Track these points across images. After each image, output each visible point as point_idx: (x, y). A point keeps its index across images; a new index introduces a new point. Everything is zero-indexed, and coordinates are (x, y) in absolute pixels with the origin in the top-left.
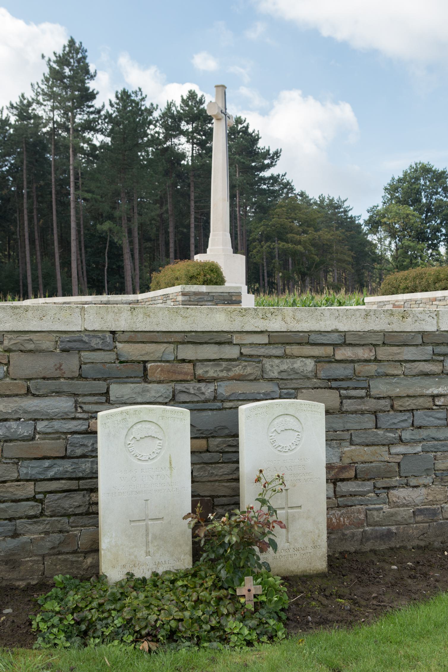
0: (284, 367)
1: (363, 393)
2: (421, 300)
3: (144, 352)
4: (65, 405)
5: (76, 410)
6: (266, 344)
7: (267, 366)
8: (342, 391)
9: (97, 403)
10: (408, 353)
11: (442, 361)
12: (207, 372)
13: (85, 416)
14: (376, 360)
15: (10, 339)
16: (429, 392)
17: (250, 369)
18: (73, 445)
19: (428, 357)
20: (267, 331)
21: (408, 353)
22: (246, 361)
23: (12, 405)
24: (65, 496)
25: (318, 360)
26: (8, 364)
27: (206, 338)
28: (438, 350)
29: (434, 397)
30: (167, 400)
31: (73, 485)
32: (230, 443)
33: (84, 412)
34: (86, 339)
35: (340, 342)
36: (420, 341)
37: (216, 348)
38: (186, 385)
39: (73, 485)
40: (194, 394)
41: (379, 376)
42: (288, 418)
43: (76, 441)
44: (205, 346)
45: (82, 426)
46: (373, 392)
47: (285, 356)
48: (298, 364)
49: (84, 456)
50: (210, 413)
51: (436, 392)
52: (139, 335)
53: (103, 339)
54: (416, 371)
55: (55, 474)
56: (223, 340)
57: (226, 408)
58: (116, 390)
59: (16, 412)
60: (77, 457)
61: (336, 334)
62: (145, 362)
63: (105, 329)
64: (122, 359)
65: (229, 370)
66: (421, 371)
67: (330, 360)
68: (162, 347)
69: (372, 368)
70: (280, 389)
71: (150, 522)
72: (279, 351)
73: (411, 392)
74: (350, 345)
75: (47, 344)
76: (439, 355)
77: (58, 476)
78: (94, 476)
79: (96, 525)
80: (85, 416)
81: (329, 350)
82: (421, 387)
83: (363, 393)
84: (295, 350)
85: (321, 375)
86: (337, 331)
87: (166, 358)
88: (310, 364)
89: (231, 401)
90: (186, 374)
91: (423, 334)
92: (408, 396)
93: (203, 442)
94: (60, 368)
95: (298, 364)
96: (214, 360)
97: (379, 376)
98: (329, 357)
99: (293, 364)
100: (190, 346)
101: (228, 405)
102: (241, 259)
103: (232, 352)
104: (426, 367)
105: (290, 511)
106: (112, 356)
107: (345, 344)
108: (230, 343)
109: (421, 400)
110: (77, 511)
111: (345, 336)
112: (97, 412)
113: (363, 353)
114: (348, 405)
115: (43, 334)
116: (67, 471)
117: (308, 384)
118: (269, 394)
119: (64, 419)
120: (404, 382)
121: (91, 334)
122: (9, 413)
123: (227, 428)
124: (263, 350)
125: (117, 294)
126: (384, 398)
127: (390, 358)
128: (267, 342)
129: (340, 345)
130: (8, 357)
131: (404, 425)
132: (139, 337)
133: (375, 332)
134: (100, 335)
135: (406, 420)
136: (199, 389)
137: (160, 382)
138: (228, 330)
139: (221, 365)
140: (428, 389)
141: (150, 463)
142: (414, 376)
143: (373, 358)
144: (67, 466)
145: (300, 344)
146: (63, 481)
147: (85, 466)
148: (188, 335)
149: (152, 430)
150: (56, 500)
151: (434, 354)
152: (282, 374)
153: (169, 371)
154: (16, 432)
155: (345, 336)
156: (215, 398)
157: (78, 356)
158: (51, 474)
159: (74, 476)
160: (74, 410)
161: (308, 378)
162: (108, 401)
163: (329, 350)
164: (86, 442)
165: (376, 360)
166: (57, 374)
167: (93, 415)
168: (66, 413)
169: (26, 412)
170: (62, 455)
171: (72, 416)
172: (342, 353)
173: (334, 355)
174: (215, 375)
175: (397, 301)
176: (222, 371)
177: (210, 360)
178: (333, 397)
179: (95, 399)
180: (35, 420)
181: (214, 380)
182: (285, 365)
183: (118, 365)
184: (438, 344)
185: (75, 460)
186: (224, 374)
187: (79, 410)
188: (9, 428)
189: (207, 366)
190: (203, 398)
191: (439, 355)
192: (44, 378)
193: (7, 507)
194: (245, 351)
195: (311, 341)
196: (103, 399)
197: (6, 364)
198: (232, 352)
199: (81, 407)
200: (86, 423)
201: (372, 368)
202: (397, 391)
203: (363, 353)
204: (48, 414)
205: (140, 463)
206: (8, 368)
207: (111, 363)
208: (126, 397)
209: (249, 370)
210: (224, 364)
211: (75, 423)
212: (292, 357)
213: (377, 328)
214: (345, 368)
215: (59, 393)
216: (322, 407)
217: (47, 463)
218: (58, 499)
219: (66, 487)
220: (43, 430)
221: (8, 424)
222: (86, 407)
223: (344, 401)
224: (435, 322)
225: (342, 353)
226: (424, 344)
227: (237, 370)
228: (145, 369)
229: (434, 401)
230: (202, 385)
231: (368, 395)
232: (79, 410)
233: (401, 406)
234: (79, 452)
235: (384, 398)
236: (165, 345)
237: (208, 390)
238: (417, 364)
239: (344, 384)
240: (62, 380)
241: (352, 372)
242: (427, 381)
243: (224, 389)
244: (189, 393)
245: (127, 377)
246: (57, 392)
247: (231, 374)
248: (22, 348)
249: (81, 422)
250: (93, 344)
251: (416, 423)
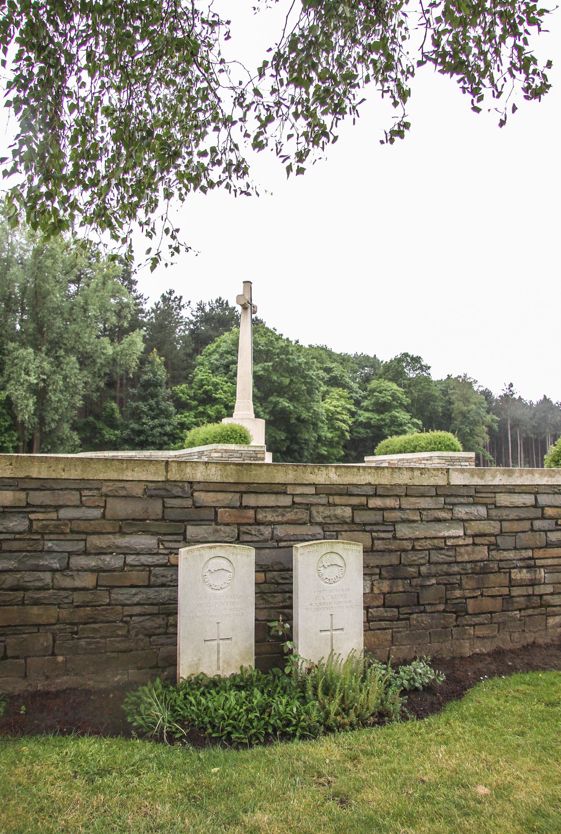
0: (327, 513)
1: (390, 535)
2: (412, 459)
3: (214, 500)
4: (150, 542)
5: (159, 547)
6: (313, 495)
7: (314, 513)
8: (373, 534)
9: (176, 541)
10: (424, 503)
11: (452, 510)
12: (266, 517)
13: (166, 552)
14: (400, 509)
15: (108, 486)
16: (441, 534)
17: (303, 515)
18: (156, 576)
19: (441, 506)
20: (314, 484)
21: (424, 503)
22: (297, 508)
23: (106, 541)
24: (148, 619)
25: (354, 508)
26: (105, 507)
27: (266, 488)
28: (448, 500)
29: (445, 538)
30: (233, 540)
31: (155, 609)
32: (283, 576)
33: (165, 548)
34: (169, 487)
35: (371, 493)
36: (434, 493)
37: (273, 497)
38: (249, 527)
39: (155, 609)
40: (255, 535)
41: (404, 521)
42: (334, 556)
43: (158, 572)
44: (265, 495)
45: (162, 560)
46: (399, 534)
47: (329, 504)
48: (339, 511)
49: (163, 585)
50: (267, 551)
51: (446, 534)
52: (212, 485)
53: (183, 488)
54: (431, 518)
55: (140, 600)
56: (279, 490)
57: (281, 547)
58: (191, 531)
59: (109, 547)
60: (158, 586)
61: (369, 487)
62: (215, 507)
63: (184, 480)
64: (198, 505)
65: (283, 515)
66: (436, 518)
67: (365, 507)
68: (230, 496)
69: (397, 515)
70: (324, 531)
71: (221, 642)
72: (324, 500)
73: (428, 535)
74: (380, 496)
75: (138, 491)
76: (450, 504)
77: (142, 602)
78: (174, 601)
79: (175, 644)
80: (166, 552)
81: (363, 500)
82: (435, 530)
83: (390, 535)
84: (337, 500)
85: (357, 520)
86: (369, 484)
87: (232, 504)
88: (348, 512)
89: (285, 541)
90: (249, 518)
91: (437, 487)
92: (426, 538)
93: (262, 575)
94: (146, 511)
95: (339, 511)
96: (272, 507)
97: (404, 521)
98: (364, 506)
99: (334, 511)
100: (253, 495)
101: (282, 544)
102: (261, 423)
103: (286, 501)
104: (439, 514)
105: (334, 632)
106: (189, 503)
107: (375, 495)
108: (285, 493)
109: (436, 541)
110: (158, 631)
111: (376, 488)
112: (178, 549)
113: (390, 502)
114: (379, 545)
115: (134, 483)
116: (149, 598)
117: (346, 527)
118: (315, 535)
119: (149, 554)
120: (422, 526)
121: (173, 483)
122: (104, 548)
123: (281, 564)
124: (311, 499)
125: (142, 449)
126: (406, 539)
127: (412, 507)
128: (314, 492)
129: (372, 496)
130: (105, 501)
131: (422, 561)
132: (212, 487)
133: (400, 485)
134: (180, 484)
135: (424, 557)
136: (259, 530)
137: (228, 524)
138: (283, 482)
139: (277, 511)
140: (440, 532)
141: (222, 591)
142: (430, 521)
143: (397, 507)
144: (151, 593)
145: (340, 495)
146: (146, 607)
147: (165, 593)
148: (251, 486)
149: (340, 562)
150: (140, 622)
151: (445, 503)
152: (327, 519)
153: (235, 516)
154: (109, 564)
155: (376, 488)
156: (272, 539)
157: (161, 501)
158: (136, 599)
159: (155, 601)
160: (157, 546)
161: (346, 523)
162: (185, 539)
163: (363, 500)
164: (165, 573)
165: (400, 509)
166: (144, 516)
167: (175, 551)
168: (150, 549)
169: (118, 547)
170: (146, 584)
171: (155, 551)
172: (375, 502)
173: (367, 504)
174: (272, 519)
175: (392, 460)
176: (278, 516)
177: (268, 507)
178: (367, 537)
179: (175, 537)
180: (125, 554)
181: (271, 523)
182: (328, 512)
183: (194, 510)
184: (448, 496)
185: (157, 589)
186: (280, 519)
187: (161, 547)
188: (104, 560)
189: (265, 512)
190: (262, 538)
191: (450, 504)
192: (133, 520)
193: (100, 627)
194: (297, 500)
195: (349, 493)
196: (181, 538)
197: (102, 507)
198: (286, 501)
199: (162, 544)
200: (167, 557)
201: (397, 515)
202: (417, 534)
203: (390, 502)
204: (136, 549)
205: (213, 591)
206: (104, 511)
207: (188, 508)
208: (200, 537)
209: (299, 516)
210: (280, 510)
211: (156, 557)
212: (335, 505)
213: (400, 482)
214: (376, 515)
215: (145, 532)
216: (361, 548)
217: (134, 591)
218: (143, 621)
219: (148, 611)
220: (132, 563)
221: (103, 557)
222: (167, 545)
223: (375, 542)
224: (446, 477)
225: (375, 502)
226: (437, 495)
227: (290, 516)
228: (216, 513)
229: (445, 542)
230: (261, 527)
231: (395, 538)
232: (161, 547)
233: (420, 546)
234: (160, 580)
235: (406, 539)
236: (232, 494)
237: (267, 531)
238: (433, 511)
239: (375, 528)
240: (148, 521)
241: (381, 518)
242: (437, 526)
243: (280, 531)
244: (251, 534)
245: (201, 520)
246: (143, 531)
247: (285, 519)
248: (116, 494)
249: (162, 556)
250: (174, 492)
251: (431, 561)
